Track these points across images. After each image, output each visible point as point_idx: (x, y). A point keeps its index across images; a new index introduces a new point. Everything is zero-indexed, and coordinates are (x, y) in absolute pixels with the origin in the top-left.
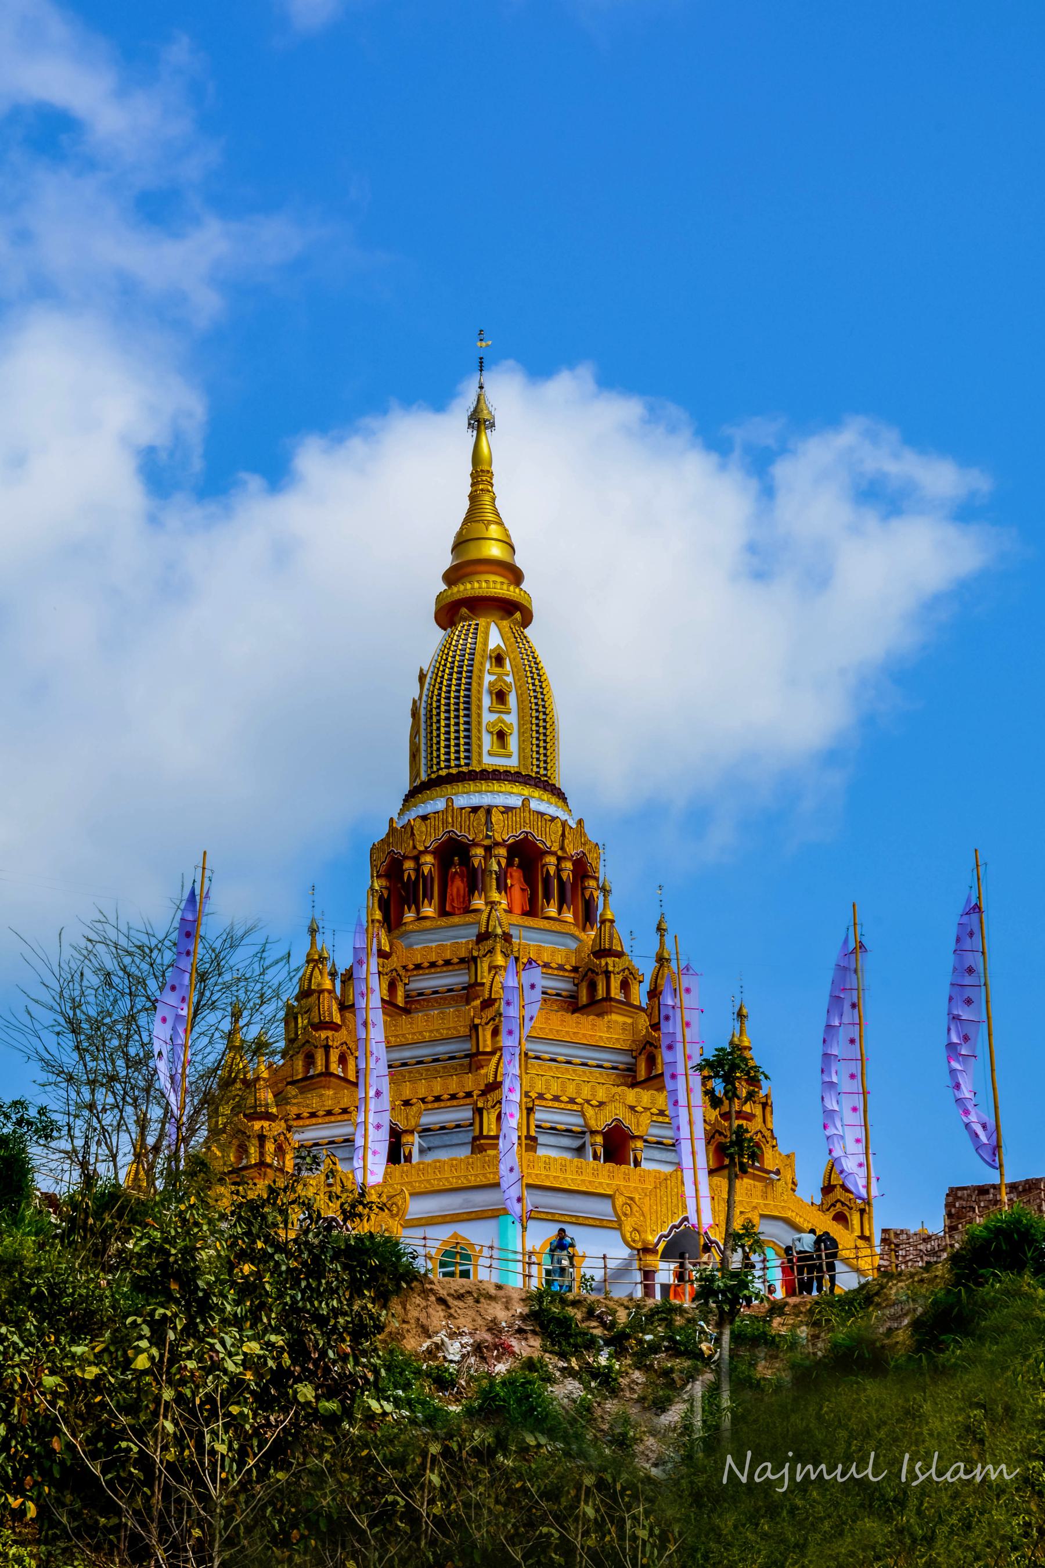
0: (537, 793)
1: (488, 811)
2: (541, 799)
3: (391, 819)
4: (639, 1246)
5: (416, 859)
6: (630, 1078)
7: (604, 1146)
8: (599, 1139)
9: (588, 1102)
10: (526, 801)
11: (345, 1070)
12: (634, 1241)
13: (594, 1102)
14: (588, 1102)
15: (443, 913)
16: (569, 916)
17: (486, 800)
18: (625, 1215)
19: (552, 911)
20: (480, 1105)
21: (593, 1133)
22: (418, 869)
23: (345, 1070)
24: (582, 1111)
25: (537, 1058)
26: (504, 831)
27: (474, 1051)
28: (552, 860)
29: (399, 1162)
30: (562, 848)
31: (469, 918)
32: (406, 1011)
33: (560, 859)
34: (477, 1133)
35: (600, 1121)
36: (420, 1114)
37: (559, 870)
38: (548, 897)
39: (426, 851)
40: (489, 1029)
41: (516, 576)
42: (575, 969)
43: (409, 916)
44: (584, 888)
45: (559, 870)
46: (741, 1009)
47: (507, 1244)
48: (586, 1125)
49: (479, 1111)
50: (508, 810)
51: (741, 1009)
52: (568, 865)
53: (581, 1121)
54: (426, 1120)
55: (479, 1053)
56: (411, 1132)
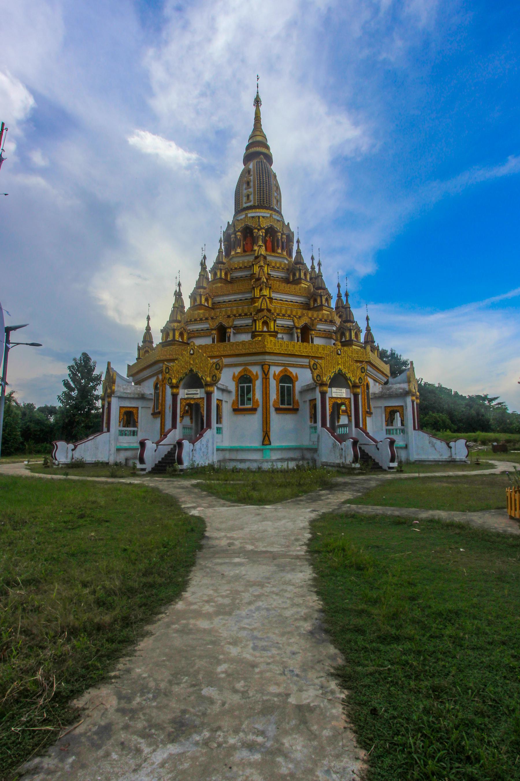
0: (250, 211)
1: (259, 217)
2: (275, 215)
3: (228, 222)
4: (320, 382)
5: (235, 234)
6: (306, 307)
7: (301, 333)
8: (299, 331)
9: (295, 316)
10: (271, 215)
11: (208, 303)
12: (317, 380)
13: (297, 317)
14: (295, 316)
15: (244, 251)
16: (285, 253)
17: (258, 214)
18: (314, 369)
19: (279, 251)
20: (255, 318)
21: (297, 328)
22: (236, 237)
23: (208, 303)
24: (293, 320)
25: (275, 299)
26: (265, 224)
27: (253, 296)
28: (280, 234)
29: (225, 341)
30: (283, 231)
31: (252, 253)
32: (231, 282)
33: (282, 234)
34: (254, 330)
35: (300, 323)
36: (234, 320)
37: (282, 238)
38: (278, 247)
39: (238, 231)
40: (259, 288)
41: (268, 147)
42: (288, 269)
43: (233, 253)
44: (289, 245)
45: (282, 238)
46: (15, 328)
47: (265, 346)
48: (294, 325)
49: (255, 321)
50: (263, 217)
51: (15, 328)
52: (285, 236)
53: (292, 323)
54: (237, 323)
55: (254, 298)
56: (230, 328)
